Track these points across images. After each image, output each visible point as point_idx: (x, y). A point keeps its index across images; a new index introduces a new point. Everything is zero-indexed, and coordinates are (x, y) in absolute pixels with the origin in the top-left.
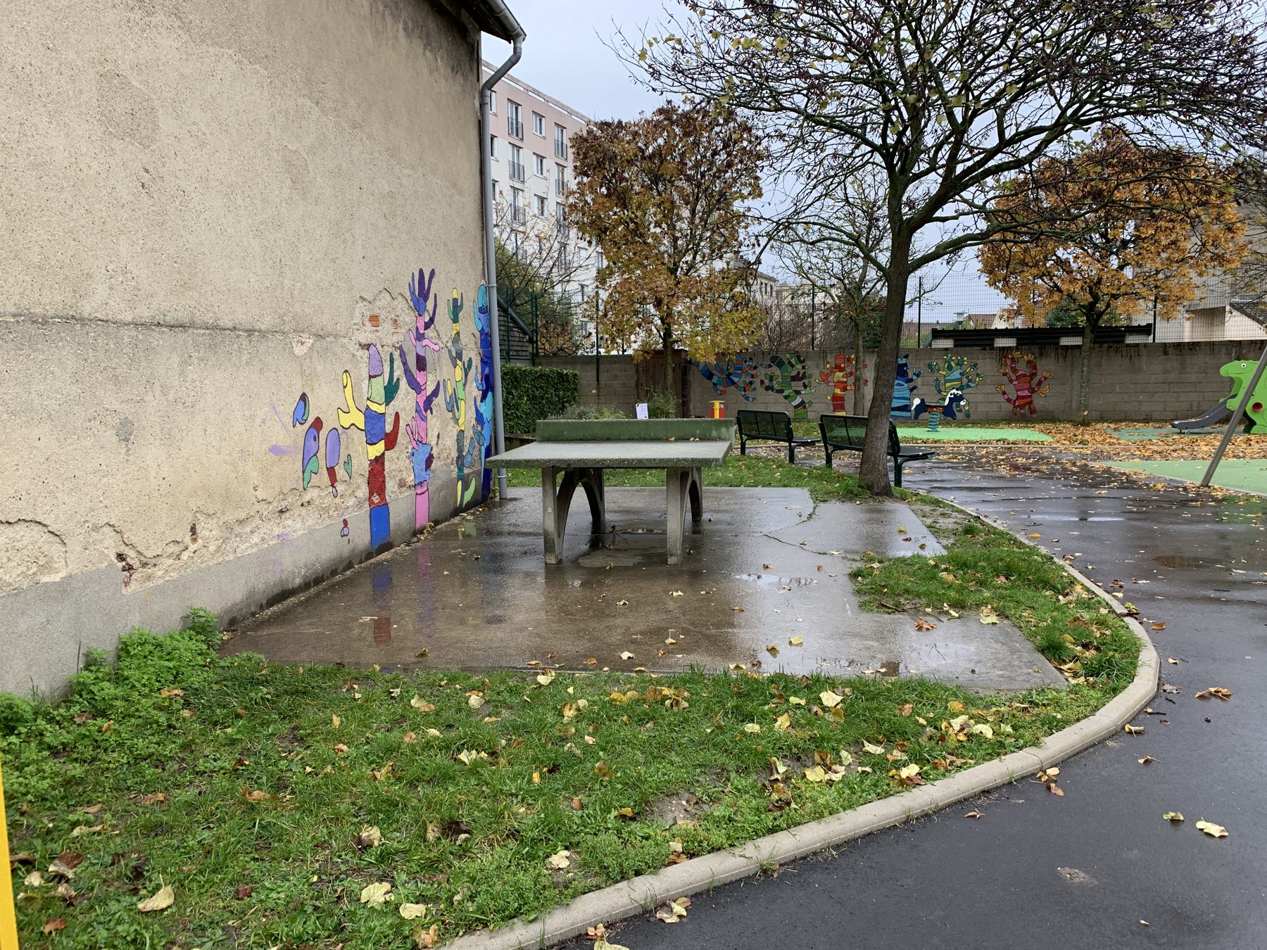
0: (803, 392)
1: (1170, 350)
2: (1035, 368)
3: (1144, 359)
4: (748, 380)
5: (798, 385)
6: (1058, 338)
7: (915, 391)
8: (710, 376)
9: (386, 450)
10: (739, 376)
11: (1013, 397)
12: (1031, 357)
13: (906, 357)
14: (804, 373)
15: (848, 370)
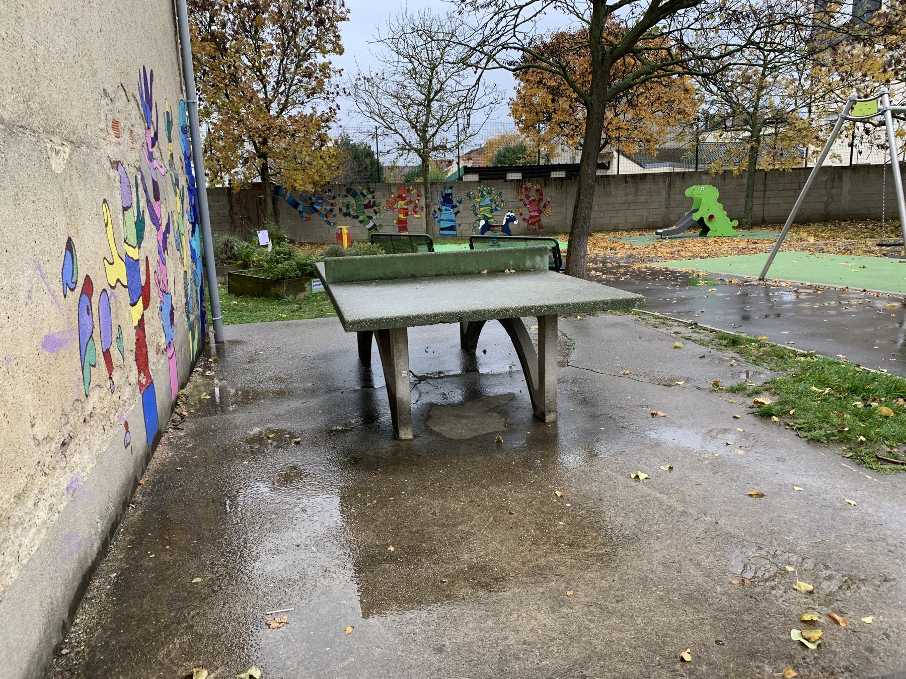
0: (374, 217)
1: (629, 179)
2: (542, 195)
3: (612, 186)
4: (329, 208)
6: (549, 172)
7: (458, 215)
8: (296, 205)
9: (144, 309)
10: (321, 204)
11: (527, 217)
12: (538, 187)
13: (451, 188)
14: (374, 202)
15: (408, 199)
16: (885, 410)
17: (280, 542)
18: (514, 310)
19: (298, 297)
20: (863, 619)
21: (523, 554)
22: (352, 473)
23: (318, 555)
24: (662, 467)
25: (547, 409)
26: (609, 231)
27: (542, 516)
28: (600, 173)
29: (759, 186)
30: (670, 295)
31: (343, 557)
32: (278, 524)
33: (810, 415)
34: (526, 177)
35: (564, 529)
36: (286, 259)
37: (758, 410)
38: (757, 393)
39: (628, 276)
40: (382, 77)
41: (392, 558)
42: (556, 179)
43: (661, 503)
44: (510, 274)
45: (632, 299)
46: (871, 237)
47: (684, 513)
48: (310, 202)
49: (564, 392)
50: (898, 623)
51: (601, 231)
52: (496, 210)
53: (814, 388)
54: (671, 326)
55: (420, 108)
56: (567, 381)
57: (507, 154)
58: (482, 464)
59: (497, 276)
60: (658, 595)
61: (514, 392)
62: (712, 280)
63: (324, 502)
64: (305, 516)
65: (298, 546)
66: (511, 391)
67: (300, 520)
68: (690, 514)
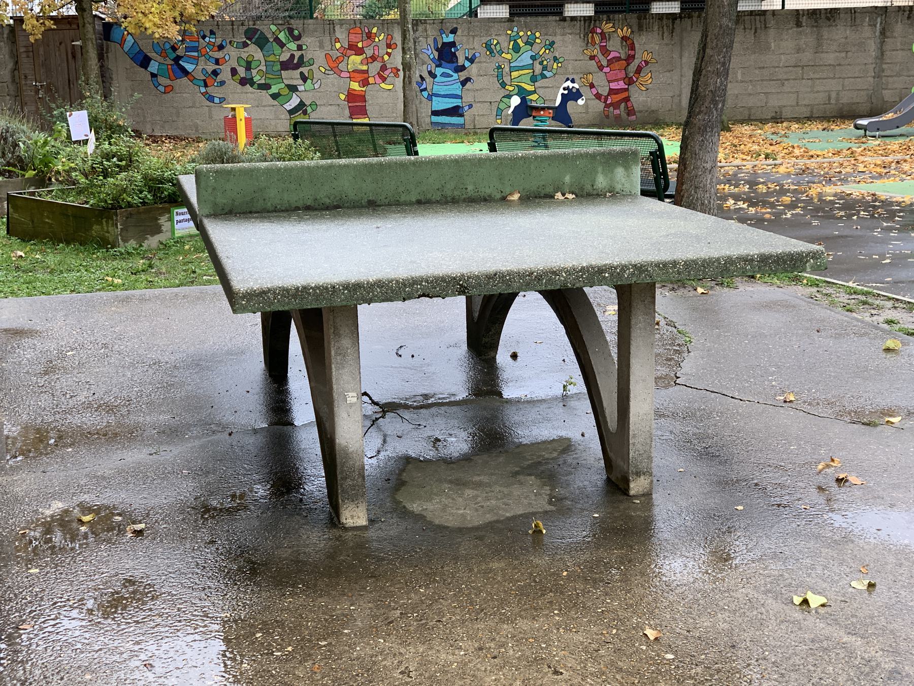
1: (804, 20)
4: (211, 67)
5: (291, 76)
7: (468, 85)
11: (604, 91)
12: (626, 31)
13: (454, 31)
14: (302, 57)
15: (369, 52)
19: (145, 245)
22: (245, 593)
25: (632, 469)
26: (763, 121)
27: (618, 677)
34: (603, 12)
36: (122, 169)
39: (798, 211)
42: (661, 17)
43: (851, 654)
48: (174, 55)
51: (747, 120)
52: (544, 77)
54: (879, 308)
56: (674, 415)
59: (539, 205)
64: (150, 676)
66: (564, 433)
68: (908, 675)
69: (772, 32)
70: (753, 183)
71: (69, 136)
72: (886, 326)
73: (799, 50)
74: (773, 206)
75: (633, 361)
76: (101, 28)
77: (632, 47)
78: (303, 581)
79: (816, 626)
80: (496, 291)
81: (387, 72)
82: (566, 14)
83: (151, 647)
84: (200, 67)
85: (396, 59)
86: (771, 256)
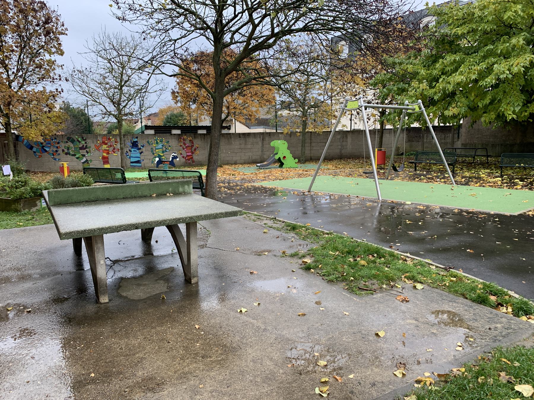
1: (241, 136)
4: (55, 149)
5: (84, 152)
6: (197, 130)
7: (142, 154)
8: (31, 148)
10: (50, 147)
11: (185, 156)
12: (191, 138)
13: (137, 138)
14: (86, 146)
15: (109, 144)
16: (363, 262)
17: (15, 381)
18: (169, 220)
19: (31, 210)
20: (349, 377)
21: (175, 367)
22: (67, 329)
23: (42, 386)
24: (254, 304)
25: (192, 276)
26: (232, 164)
27: (187, 341)
28: (225, 131)
29: (308, 140)
30: (263, 202)
31: (60, 385)
32: (14, 369)
33: (329, 267)
34: (184, 133)
35: (199, 348)
36: (23, 186)
37: (304, 266)
38: (304, 256)
39: (241, 191)
40: (90, 71)
41: (93, 381)
42: (201, 134)
43: (253, 325)
44: (170, 196)
45: (236, 211)
46: (362, 168)
47: (265, 330)
48: (41, 146)
49: (203, 264)
50: (365, 376)
51: (227, 164)
52: (166, 151)
53: (331, 252)
54: (262, 220)
55: (116, 90)
56: (205, 257)
57: (172, 118)
58: (153, 314)
59: (162, 198)
60: (250, 380)
61: (174, 266)
62: (286, 192)
63: (47, 351)
64: (34, 361)
65: (28, 382)
66: (172, 266)
67: (30, 364)
68: (268, 330)
69: (233, 139)
70: (229, 183)
71: (3, 174)
72: (264, 225)
73: (240, 144)
74: (234, 190)
75: (191, 244)
76: (15, 137)
77: (193, 143)
78: (87, 323)
79: (244, 318)
80: (147, 227)
81: (115, 150)
82: (172, 133)
83: (34, 351)
84: (51, 149)
85: (118, 146)
86: (228, 212)
